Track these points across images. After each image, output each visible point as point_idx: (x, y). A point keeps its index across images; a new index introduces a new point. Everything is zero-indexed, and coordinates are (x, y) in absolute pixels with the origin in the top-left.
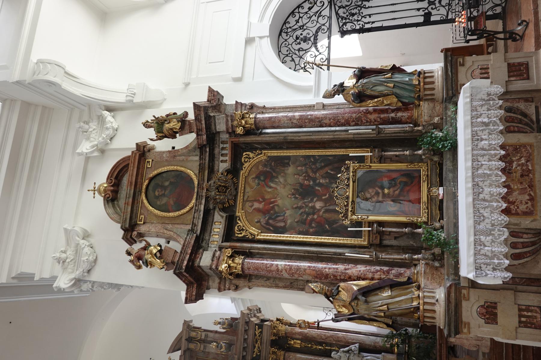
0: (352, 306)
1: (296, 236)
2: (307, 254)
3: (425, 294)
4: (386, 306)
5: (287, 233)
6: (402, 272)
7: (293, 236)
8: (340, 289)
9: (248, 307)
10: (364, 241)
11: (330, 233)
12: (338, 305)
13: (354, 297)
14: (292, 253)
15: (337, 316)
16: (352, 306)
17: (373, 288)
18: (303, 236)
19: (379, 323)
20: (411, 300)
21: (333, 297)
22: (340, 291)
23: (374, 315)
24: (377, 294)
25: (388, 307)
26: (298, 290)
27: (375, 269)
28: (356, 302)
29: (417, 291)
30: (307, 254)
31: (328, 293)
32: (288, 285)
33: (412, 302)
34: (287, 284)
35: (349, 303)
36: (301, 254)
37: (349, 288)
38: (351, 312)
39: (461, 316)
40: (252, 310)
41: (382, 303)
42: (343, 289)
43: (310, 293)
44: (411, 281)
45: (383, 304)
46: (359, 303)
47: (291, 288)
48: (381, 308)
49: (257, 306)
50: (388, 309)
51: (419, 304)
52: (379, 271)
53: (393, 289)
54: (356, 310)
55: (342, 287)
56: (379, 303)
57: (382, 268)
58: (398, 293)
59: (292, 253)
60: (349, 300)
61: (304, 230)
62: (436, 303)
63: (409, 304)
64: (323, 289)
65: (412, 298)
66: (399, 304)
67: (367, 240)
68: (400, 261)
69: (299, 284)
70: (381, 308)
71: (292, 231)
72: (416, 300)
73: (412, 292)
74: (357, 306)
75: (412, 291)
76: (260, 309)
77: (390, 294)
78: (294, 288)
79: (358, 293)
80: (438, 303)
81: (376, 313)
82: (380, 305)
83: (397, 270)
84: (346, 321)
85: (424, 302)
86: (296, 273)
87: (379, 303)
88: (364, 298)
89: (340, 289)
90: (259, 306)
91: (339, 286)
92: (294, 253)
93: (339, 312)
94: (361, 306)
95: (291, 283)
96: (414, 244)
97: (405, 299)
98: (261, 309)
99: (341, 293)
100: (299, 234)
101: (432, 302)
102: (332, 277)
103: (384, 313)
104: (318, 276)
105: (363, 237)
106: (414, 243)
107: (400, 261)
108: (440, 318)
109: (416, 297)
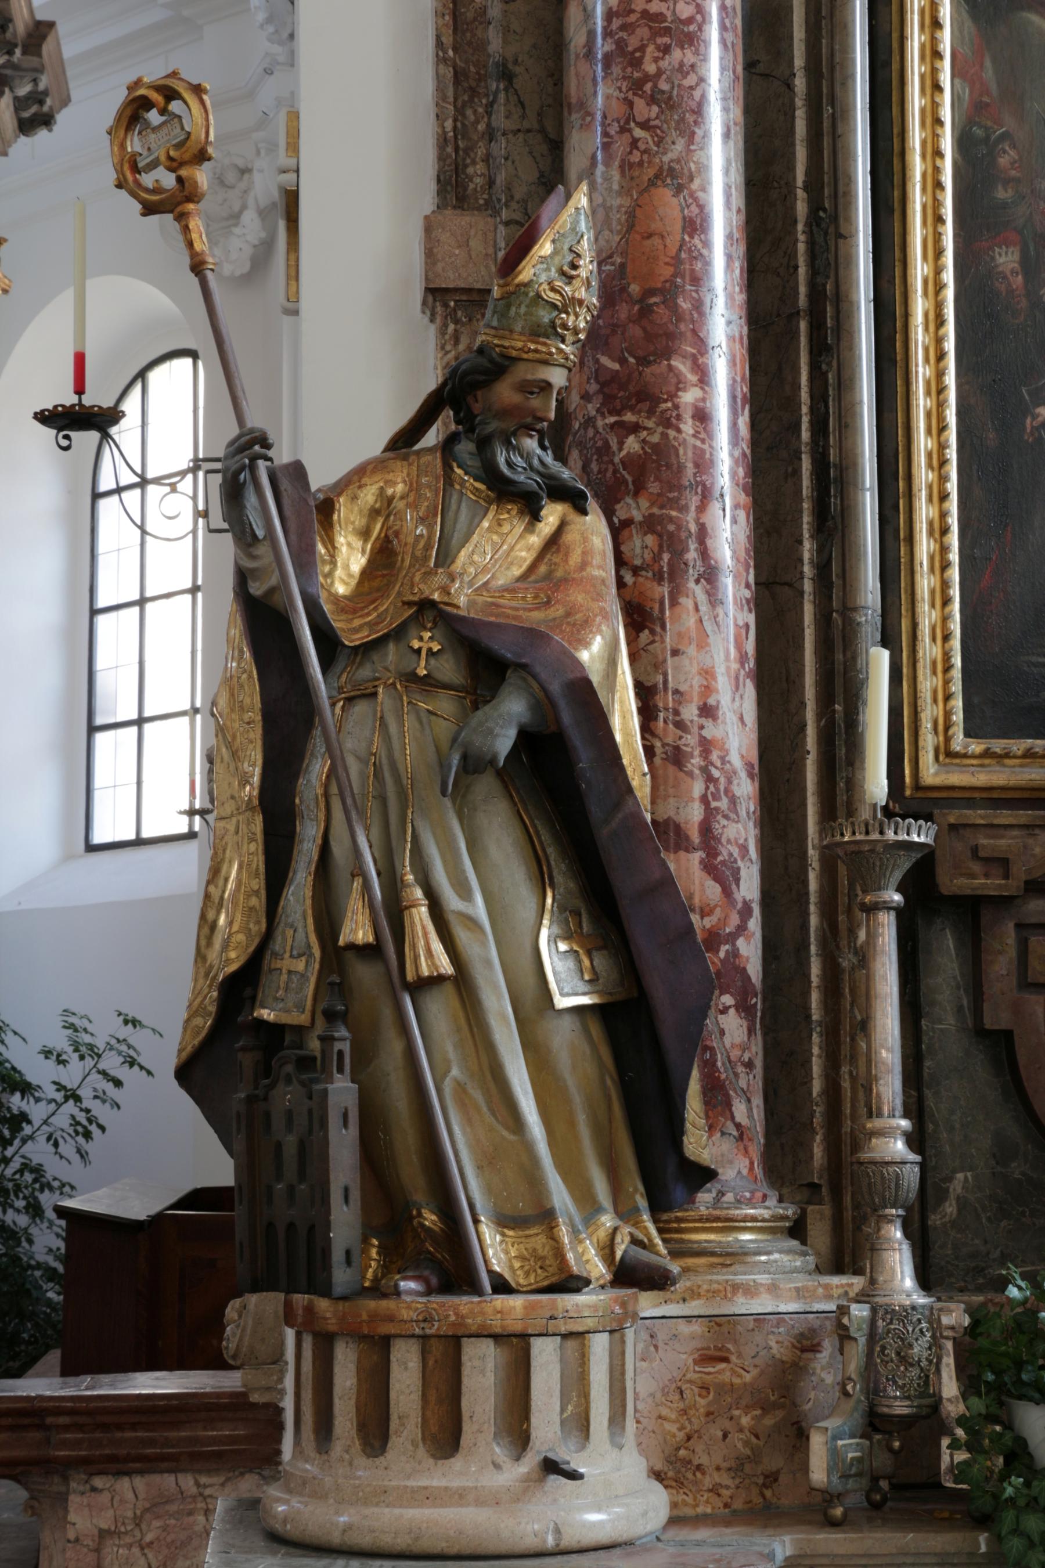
0: (398, 634)
1: (946, 114)
2: (801, 208)
3: (600, 1345)
4: (446, 966)
5: (969, 24)
6: (740, 1109)
7: (946, 78)
8: (552, 514)
9: (51, 25)
10: (946, 754)
11: (991, 437)
12: (384, 508)
13: (504, 647)
14: (799, 61)
15: (285, 485)
16: (398, 634)
17: (603, 833)
18: (947, 178)
19: (258, 903)
20: (523, 1207)
21: (465, 448)
22: (535, 516)
23: (339, 851)
24: (542, 879)
25: (438, 980)
26: (442, 141)
27: (744, 849)
28: (449, 669)
29: (607, 1250)
30: (801, 208)
31: (505, 393)
32: (481, 46)
33: (504, 1222)
34: (495, 44)
35: (426, 605)
36: (801, 154)
37: (578, 597)
38: (338, 624)
39: (154, 1472)
40: (32, 61)
41: (472, 922)
42: (553, 542)
43: (430, 254)
44: (678, 1192)
45: (462, 936)
46: (445, 704)
47: (459, 76)
48: (421, 915)
49: (66, 101)
50: (422, 986)
51: (502, 1286)
52: (727, 893)
53: (596, 1029)
54: (365, 672)
55: (570, 537)
56: (465, 893)
57: (754, 924)
58: (571, 1082)
59: (799, 61)
60: (462, 598)
61: (1002, 194)
62: (529, 1463)
63: (489, 1190)
64: (553, 331)
65: (546, 1217)
66: (477, 1095)
67: (956, 778)
68: (817, 1086)
69: (500, 147)
70: (421, 915)
71: (989, 73)
72: (532, 1259)
73: (590, 1207)
74: (411, 678)
75: (599, 1210)
76: (46, 121)
77: (562, 1002)
78: (460, 112)
79: (555, 687)
80: (526, 1479)
81: (359, 871)
82: (452, 901)
83: (749, 1065)
84: (242, 577)
85: (524, 1338)
86: (637, 86)
87: (465, 893)
88: (504, 743)
89: (552, 514)
90: (61, 118)
91: (577, 501)
92: (800, 83)
93: (326, 508)
94: (409, 721)
95: (507, 76)
96: (950, 1208)
97: (529, 1147)
98: (43, 134)
99: (514, 524)
100: (962, 142)
101: (537, 1420)
102: (632, 444)
103: (372, 951)
104: (623, 311)
105: (976, 747)
106: (962, 1204)
107: (817, 1086)
108: (380, 1496)
109: (559, 1253)
